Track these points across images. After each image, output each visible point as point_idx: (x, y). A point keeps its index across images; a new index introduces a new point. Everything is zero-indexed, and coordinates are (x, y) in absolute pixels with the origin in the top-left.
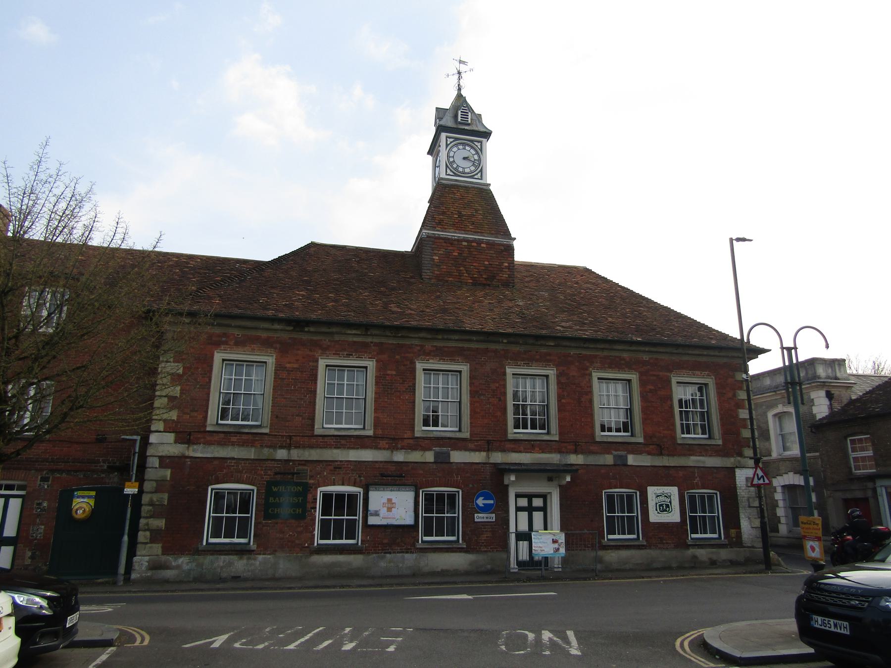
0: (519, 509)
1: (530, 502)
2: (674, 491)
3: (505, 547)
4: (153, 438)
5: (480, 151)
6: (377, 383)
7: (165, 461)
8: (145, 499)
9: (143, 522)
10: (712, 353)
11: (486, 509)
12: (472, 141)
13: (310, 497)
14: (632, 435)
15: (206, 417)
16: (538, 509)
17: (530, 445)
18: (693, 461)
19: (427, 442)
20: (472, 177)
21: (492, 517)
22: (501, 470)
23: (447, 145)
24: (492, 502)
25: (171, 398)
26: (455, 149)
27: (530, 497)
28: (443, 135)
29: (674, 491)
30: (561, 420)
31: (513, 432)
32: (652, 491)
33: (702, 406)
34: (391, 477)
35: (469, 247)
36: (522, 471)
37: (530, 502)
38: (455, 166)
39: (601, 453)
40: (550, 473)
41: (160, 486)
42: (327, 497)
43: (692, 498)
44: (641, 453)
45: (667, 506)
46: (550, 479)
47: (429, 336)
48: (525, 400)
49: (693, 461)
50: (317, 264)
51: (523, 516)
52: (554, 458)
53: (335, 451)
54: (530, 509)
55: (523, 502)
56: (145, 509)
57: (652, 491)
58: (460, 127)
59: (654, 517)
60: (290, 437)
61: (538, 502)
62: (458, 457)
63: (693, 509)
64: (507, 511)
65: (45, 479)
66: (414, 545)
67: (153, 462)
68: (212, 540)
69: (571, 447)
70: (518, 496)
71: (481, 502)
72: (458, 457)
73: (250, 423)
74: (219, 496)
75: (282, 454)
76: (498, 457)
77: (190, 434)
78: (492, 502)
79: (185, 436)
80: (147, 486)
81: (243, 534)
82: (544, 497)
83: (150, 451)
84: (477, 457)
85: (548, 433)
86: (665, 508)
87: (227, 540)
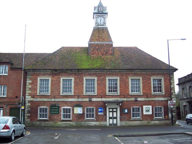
0: (109, 112)
1: (113, 110)
2: (150, 107)
3: (106, 120)
4: (27, 97)
5: (105, 18)
6: (74, 83)
7: (29, 102)
8: (26, 110)
9: (26, 114)
10: (162, 71)
11: (101, 112)
12: (102, 16)
13: (60, 109)
14: (162, 93)
15: (37, 92)
16: (115, 112)
17: (113, 96)
18: (156, 99)
19: (87, 96)
20: (103, 26)
21: (102, 114)
22: (105, 103)
23: (96, 18)
24: (102, 110)
25: (30, 88)
26: (98, 18)
27: (113, 109)
28: (95, 15)
29: (150, 107)
30: (120, 90)
31: (108, 93)
32: (144, 107)
33: (91, 85)
34: (78, 105)
35: (101, 45)
36: (109, 102)
37: (113, 110)
38: (98, 23)
39: (131, 98)
40: (118, 103)
41: (29, 107)
42: (64, 109)
43: (156, 108)
44: (142, 97)
45: (148, 110)
46: (117, 104)
47: (86, 71)
48: (156, 85)
49: (156, 99)
50: (66, 53)
51: (111, 113)
52: (119, 99)
53: (65, 99)
54: (113, 112)
55: (111, 110)
56: (26, 112)
57: (144, 107)
58: (100, 12)
59: (145, 113)
60: (55, 96)
61: (111, 110)
62: (94, 99)
63: (156, 111)
64: (106, 112)
65: (7, 106)
66: (84, 120)
67: (27, 102)
68: (40, 118)
69: (123, 96)
70: (109, 109)
71: (100, 110)
72: (94, 99)
73: (46, 93)
74: (41, 109)
75: (53, 100)
76: (104, 99)
77: (55, 96)
78: (102, 110)
79: (33, 97)
80: (26, 107)
81: (93, 117)
82: (116, 109)
83: (26, 100)
84: (99, 99)
85: (162, 93)
86: (148, 111)
87: (42, 119)
